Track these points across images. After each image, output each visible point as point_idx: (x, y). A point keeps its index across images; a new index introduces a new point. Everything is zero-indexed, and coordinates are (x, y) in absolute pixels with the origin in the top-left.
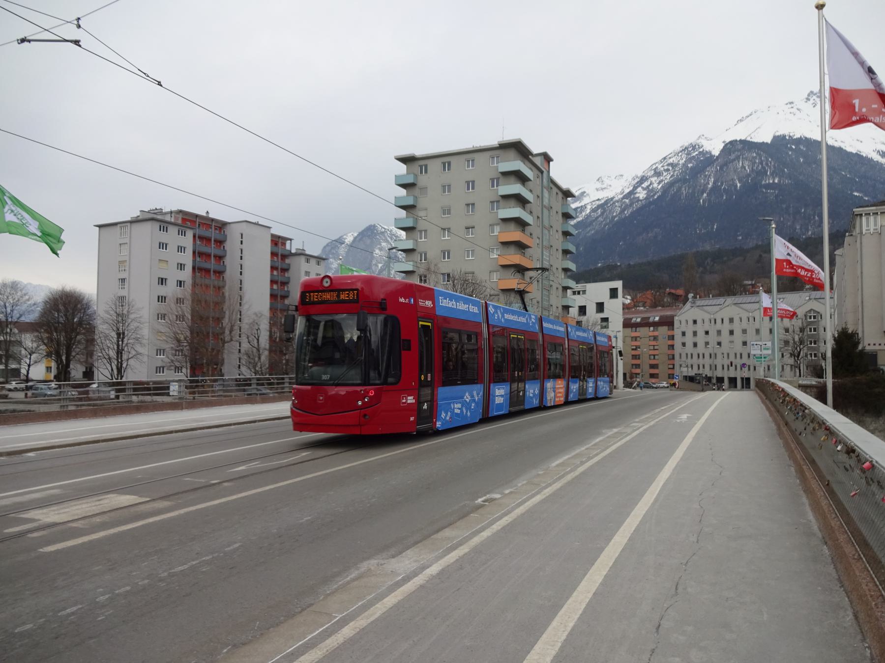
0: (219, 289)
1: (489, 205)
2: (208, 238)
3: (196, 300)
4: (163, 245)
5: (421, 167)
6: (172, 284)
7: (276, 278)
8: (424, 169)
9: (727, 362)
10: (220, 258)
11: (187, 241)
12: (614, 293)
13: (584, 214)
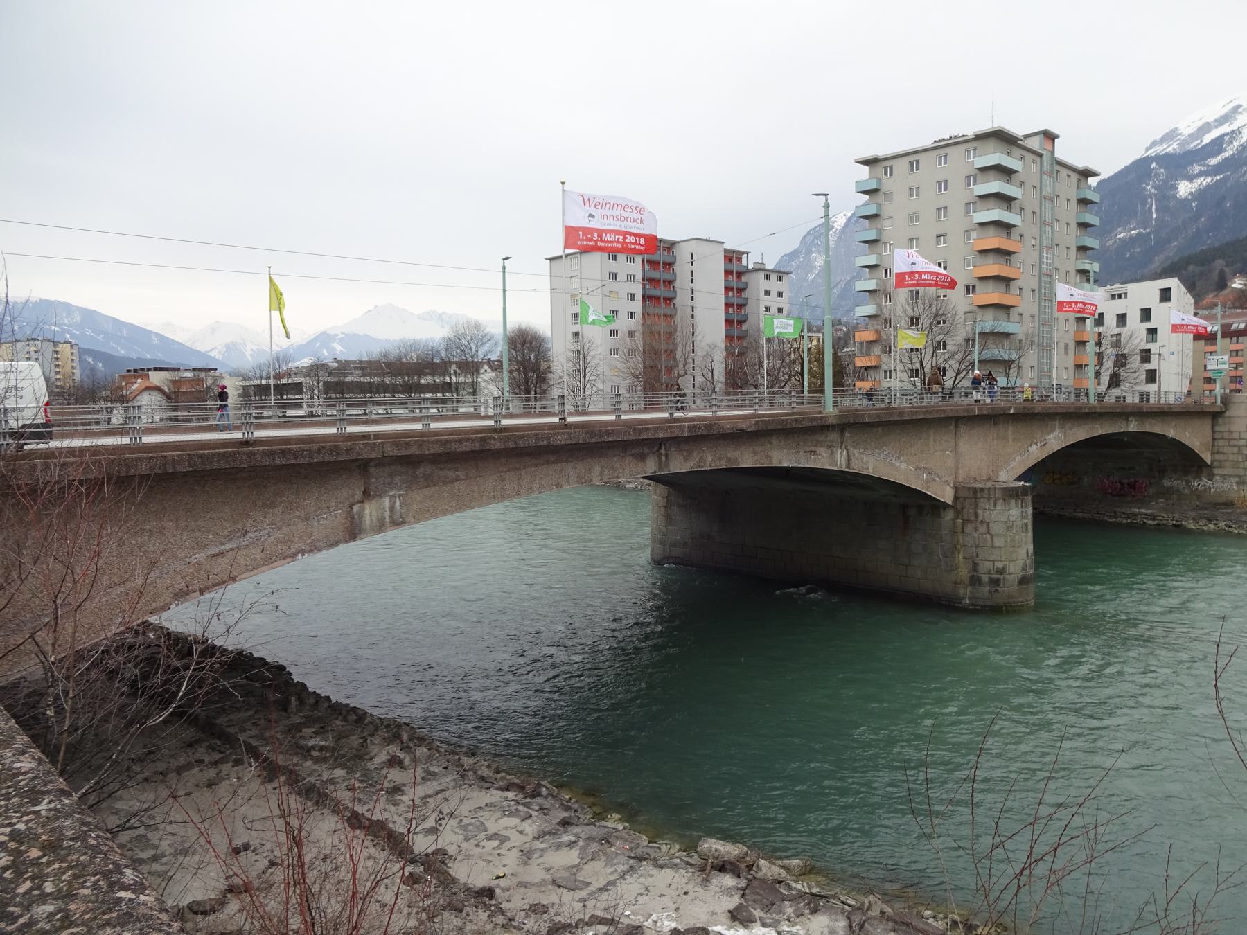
0: (670, 317)
1: (963, 208)
2: (657, 260)
3: (649, 332)
4: (612, 276)
5: (886, 168)
6: (623, 315)
7: (731, 301)
8: (889, 171)
10: (669, 283)
11: (636, 268)
12: (1165, 295)
13: (1236, 144)
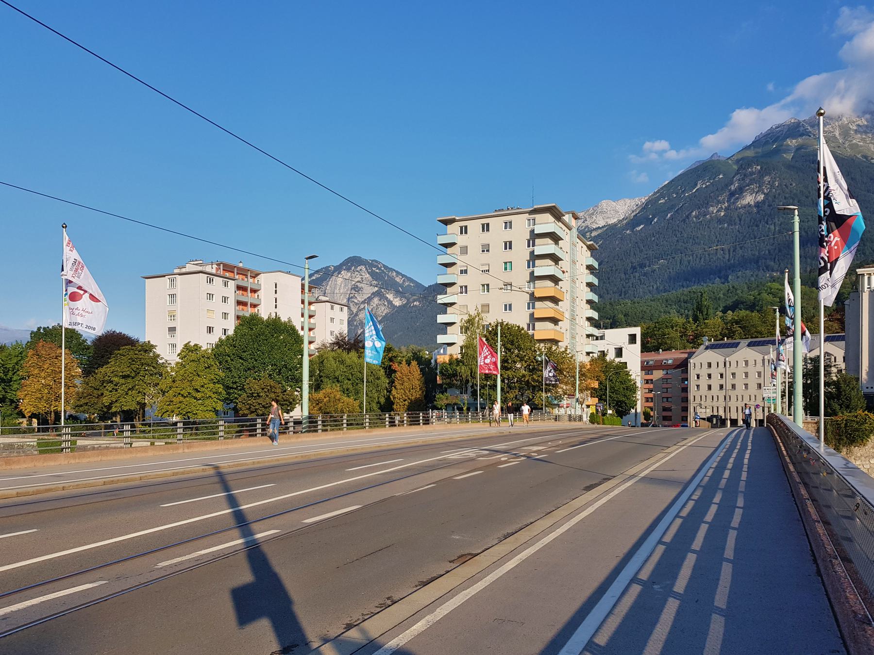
4: (210, 296)
9: (740, 404)
12: (632, 339)
